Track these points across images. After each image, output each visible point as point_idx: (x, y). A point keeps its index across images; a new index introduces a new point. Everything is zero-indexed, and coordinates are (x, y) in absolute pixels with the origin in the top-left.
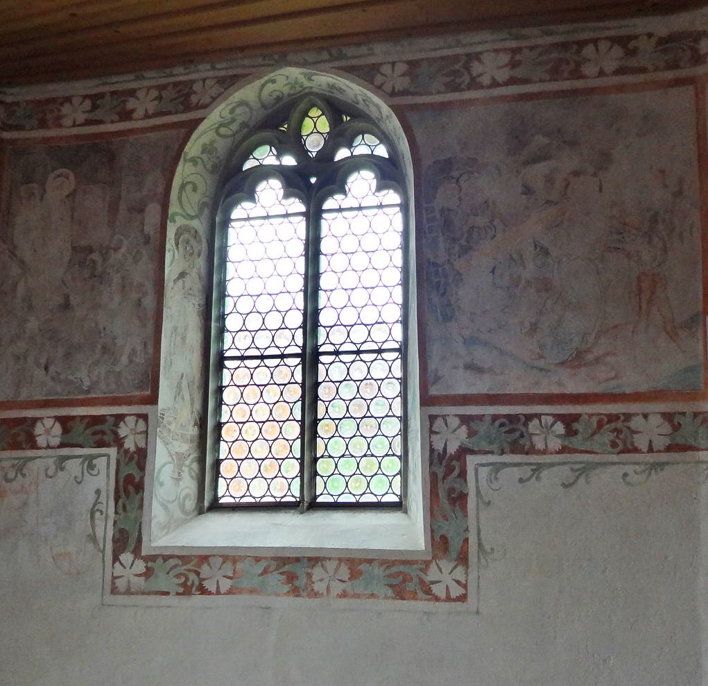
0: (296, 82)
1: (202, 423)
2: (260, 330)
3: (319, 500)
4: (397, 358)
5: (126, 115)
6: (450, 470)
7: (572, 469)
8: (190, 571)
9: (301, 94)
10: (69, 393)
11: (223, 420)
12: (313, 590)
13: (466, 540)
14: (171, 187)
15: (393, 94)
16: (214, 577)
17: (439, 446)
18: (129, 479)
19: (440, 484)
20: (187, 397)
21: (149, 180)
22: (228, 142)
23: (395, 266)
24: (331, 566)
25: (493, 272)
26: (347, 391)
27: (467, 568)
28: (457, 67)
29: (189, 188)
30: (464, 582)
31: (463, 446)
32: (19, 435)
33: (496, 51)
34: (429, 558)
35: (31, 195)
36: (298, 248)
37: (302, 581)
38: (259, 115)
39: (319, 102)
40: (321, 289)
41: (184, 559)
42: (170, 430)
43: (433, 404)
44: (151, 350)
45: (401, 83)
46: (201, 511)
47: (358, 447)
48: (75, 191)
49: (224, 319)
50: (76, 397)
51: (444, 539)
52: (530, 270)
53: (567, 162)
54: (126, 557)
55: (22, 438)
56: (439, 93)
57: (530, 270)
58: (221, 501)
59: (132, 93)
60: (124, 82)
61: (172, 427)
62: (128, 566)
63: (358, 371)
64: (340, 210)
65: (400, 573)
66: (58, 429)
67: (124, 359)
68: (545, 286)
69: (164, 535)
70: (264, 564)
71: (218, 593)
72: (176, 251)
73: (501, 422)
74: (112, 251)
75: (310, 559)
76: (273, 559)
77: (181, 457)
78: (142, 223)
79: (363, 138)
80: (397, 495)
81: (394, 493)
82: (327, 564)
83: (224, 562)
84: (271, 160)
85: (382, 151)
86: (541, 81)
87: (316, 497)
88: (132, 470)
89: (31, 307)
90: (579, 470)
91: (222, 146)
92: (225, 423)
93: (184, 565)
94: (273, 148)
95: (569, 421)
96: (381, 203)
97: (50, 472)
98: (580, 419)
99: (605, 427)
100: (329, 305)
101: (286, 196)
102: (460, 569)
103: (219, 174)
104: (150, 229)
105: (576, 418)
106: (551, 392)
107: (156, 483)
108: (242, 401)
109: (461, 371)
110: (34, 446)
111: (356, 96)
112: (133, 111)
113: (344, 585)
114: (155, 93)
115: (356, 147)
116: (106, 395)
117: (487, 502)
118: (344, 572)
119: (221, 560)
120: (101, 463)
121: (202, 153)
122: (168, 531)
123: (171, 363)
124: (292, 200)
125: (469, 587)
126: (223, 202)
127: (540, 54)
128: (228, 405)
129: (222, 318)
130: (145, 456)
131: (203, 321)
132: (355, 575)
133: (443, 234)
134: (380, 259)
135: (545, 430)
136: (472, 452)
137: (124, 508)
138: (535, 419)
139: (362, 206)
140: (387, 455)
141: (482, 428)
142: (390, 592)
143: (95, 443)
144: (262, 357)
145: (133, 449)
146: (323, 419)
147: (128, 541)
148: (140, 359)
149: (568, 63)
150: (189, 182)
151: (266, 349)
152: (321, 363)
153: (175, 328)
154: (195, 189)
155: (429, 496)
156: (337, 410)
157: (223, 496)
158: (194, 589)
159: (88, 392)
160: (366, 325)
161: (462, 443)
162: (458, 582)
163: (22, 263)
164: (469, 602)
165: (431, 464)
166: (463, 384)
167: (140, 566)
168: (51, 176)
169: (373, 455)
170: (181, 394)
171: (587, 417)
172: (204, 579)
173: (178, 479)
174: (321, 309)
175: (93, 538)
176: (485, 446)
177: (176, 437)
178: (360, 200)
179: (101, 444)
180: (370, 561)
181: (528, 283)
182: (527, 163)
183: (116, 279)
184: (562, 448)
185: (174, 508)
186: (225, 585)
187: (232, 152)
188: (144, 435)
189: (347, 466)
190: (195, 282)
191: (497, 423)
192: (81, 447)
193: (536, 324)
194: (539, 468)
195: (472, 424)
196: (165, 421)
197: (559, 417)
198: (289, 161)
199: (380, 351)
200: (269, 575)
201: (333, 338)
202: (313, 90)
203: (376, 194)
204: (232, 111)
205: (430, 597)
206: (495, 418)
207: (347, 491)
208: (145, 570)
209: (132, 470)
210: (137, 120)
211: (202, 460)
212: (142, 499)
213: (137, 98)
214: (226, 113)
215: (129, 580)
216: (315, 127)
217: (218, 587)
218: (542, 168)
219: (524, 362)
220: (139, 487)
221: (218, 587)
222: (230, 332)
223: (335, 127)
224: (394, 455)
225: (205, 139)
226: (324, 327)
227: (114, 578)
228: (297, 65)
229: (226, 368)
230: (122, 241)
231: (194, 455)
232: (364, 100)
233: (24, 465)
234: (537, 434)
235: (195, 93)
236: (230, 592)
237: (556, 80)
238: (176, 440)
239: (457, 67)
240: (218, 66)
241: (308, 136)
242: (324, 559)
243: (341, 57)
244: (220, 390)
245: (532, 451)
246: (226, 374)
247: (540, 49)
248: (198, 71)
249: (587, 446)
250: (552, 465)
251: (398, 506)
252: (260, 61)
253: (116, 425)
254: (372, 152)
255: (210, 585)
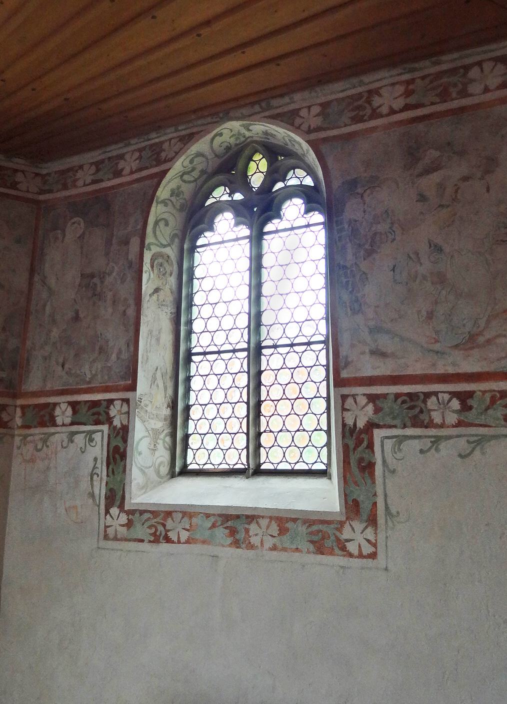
0: (239, 134)
1: (174, 405)
2: (217, 330)
3: (262, 467)
4: (323, 349)
5: (118, 174)
6: (359, 442)
7: (468, 442)
8: (158, 523)
9: (245, 143)
10: (77, 383)
11: (191, 403)
12: (250, 543)
13: (375, 504)
14: (147, 224)
15: (309, 131)
16: (177, 530)
17: (350, 422)
18: (117, 448)
19: (351, 453)
20: (161, 385)
21: (132, 220)
22: (192, 185)
23: (320, 273)
24: (264, 522)
25: (393, 270)
26: (284, 376)
27: (376, 529)
28: (360, 102)
29: (162, 224)
30: (374, 541)
31: (370, 421)
32: (44, 416)
33: (393, 84)
34: (344, 519)
35: (57, 238)
36: (245, 264)
37: (241, 536)
38: (214, 164)
39: (259, 148)
40: (263, 296)
41: (155, 513)
42: (146, 411)
43: (344, 386)
44: (132, 349)
45: (316, 122)
46: (173, 475)
47: (293, 423)
48: (84, 233)
49: (192, 324)
50: (82, 387)
51: (356, 503)
52: (425, 267)
53: (456, 170)
54: (114, 511)
55: (47, 418)
56: (346, 125)
57: (425, 267)
58: (189, 467)
59: (121, 157)
60: (114, 150)
61: (149, 409)
62: (115, 518)
63: (293, 359)
64: (277, 231)
65: (319, 531)
66: (69, 411)
67: (114, 357)
68: (440, 279)
69: (142, 494)
70: (212, 519)
71: (179, 542)
72: (151, 272)
73: (403, 399)
74: (107, 276)
75: (247, 517)
76: (220, 515)
77: (156, 433)
78: (127, 254)
79: (294, 173)
80: (324, 464)
81: (322, 462)
82: (261, 521)
83: (183, 518)
84: (226, 198)
85: (309, 181)
86: (432, 104)
87: (260, 465)
88: (118, 442)
89: (54, 322)
90: (474, 442)
91: (187, 190)
92: (192, 406)
93: (155, 518)
94: (227, 188)
95: (464, 398)
96: (308, 223)
97: (39, 447)
98: (474, 395)
99: (498, 402)
100: (269, 308)
101: (237, 224)
102: (370, 530)
103: (187, 211)
104: (132, 256)
105: (471, 394)
106: (446, 372)
107: (135, 453)
108: (204, 388)
109: (367, 357)
110: (54, 424)
111: (284, 139)
112: (122, 170)
113: (275, 540)
114: (137, 154)
115: (289, 180)
116: (101, 385)
117: (392, 470)
118: (274, 529)
119: (180, 515)
120: (97, 437)
121: (171, 196)
122: (146, 491)
123: (147, 359)
124: (241, 226)
125: (378, 545)
126: (190, 233)
127: (431, 82)
128: (194, 391)
129: (190, 322)
130: (128, 432)
131: (174, 325)
132: (283, 531)
133: (351, 241)
134: (309, 268)
135: (442, 406)
136: (378, 426)
137: (113, 472)
138: (433, 396)
139: (294, 226)
140: (316, 430)
141: (386, 405)
142: (312, 548)
143: (94, 421)
144: (219, 352)
145: (119, 426)
146: (265, 400)
147: (116, 498)
148: (125, 356)
149: (455, 85)
150: (163, 219)
151: (222, 345)
152: (263, 355)
153: (151, 332)
154: (167, 224)
155: (342, 465)
156: (276, 393)
157: (191, 464)
158: (161, 538)
159: (89, 383)
160: (298, 323)
161: (370, 419)
162: (368, 541)
163: (50, 289)
164: (378, 558)
165: (344, 437)
166: (369, 367)
167: (124, 519)
168: (69, 224)
169: (304, 430)
170: (156, 383)
171: (481, 393)
172: (169, 531)
173: (154, 450)
174: (263, 312)
175: (92, 495)
176: (389, 421)
177: (152, 416)
178: (292, 222)
179: (97, 423)
180: (295, 520)
181: (424, 278)
182: (420, 175)
183: (109, 295)
184: (458, 423)
185: (151, 473)
186: (184, 536)
187: (195, 194)
188: (127, 415)
189: (284, 439)
190: (167, 296)
191: (400, 400)
192: (85, 424)
193: (432, 312)
194: (437, 440)
195: (377, 402)
196: (142, 404)
197: (454, 394)
198: (238, 196)
199: (309, 344)
200: (217, 528)
201: (272, 335)
202: (255, 139)
203: (305, 216)
204: (191, 162)
205: (345, 553)
206: (397, 396)
207: (284, 460)
208: (127, 521)
209: (118, 442)
210: (124, 176)
211: (173, 435)
212: (125, 466)
213: (125, 160)
214: (187, 163)
215: (116, 529)
216: (258, 168)
217: (179, 537)
218: (436, 177)
219: (422, 347)
220: (123, 456)
221: (179, 537)
222: (196, 333)
223: (271, 166)
224: (321, 430)
225: (173, 185)
226: (266, 326)
227: (106, 527)
228: (237, 119)
229: (193, 362)
230: (113, 267)
231: (168, 431)
232: (290, 140)
233: (48, 438)
234: (434, 410)
235: (164, 150)
236: (188, 542)
237: (445, 101)
238: (152, 419)
239: (360, 102)
240: (180, 128)
241: (252, 175)
242: (259, 517)
243: (269, 108)
244: (188, 379)
245: (430, 425)
246: (193, 366)
247: (432, 77)
248: (166, 134)
249: (482, 420)
250: (449, 438)
251: (323, 473)
252: (209, 120)
253: (108, 407)
254: (301, 182)
255: (172, 535)
